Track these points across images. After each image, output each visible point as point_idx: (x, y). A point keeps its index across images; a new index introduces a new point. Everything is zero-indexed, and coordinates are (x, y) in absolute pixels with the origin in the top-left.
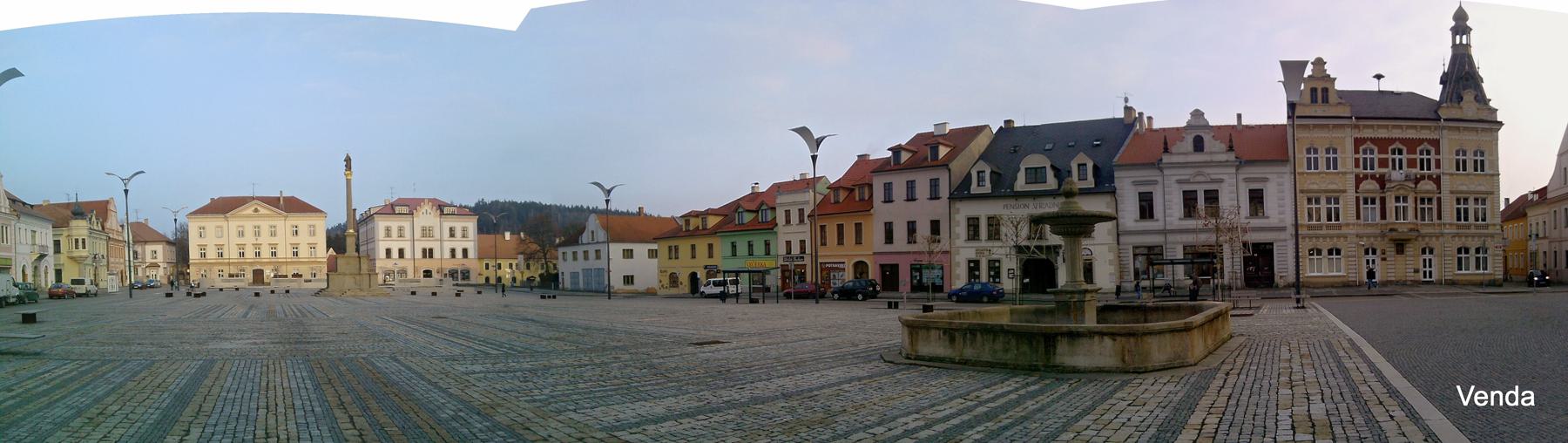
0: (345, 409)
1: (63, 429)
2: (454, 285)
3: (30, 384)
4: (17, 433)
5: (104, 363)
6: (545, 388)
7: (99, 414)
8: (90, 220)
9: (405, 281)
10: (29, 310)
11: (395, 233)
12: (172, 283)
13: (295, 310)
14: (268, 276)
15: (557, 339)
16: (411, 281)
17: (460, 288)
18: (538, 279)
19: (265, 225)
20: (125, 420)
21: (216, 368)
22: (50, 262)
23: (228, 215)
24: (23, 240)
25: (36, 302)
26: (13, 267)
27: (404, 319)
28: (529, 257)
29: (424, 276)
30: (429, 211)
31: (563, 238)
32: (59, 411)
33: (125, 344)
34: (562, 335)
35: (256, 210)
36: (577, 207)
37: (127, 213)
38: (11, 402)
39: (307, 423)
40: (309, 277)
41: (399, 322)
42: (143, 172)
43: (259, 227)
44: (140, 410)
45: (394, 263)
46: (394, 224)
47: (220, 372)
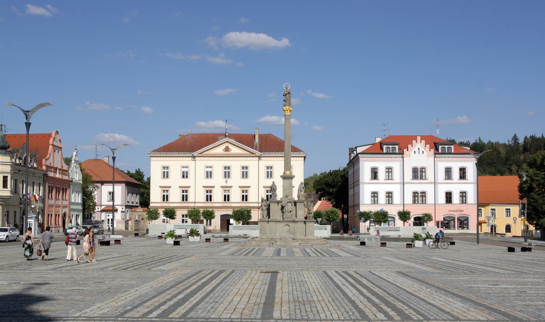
19: (236, 165)
23: (195, 154)
35: (227, 149)
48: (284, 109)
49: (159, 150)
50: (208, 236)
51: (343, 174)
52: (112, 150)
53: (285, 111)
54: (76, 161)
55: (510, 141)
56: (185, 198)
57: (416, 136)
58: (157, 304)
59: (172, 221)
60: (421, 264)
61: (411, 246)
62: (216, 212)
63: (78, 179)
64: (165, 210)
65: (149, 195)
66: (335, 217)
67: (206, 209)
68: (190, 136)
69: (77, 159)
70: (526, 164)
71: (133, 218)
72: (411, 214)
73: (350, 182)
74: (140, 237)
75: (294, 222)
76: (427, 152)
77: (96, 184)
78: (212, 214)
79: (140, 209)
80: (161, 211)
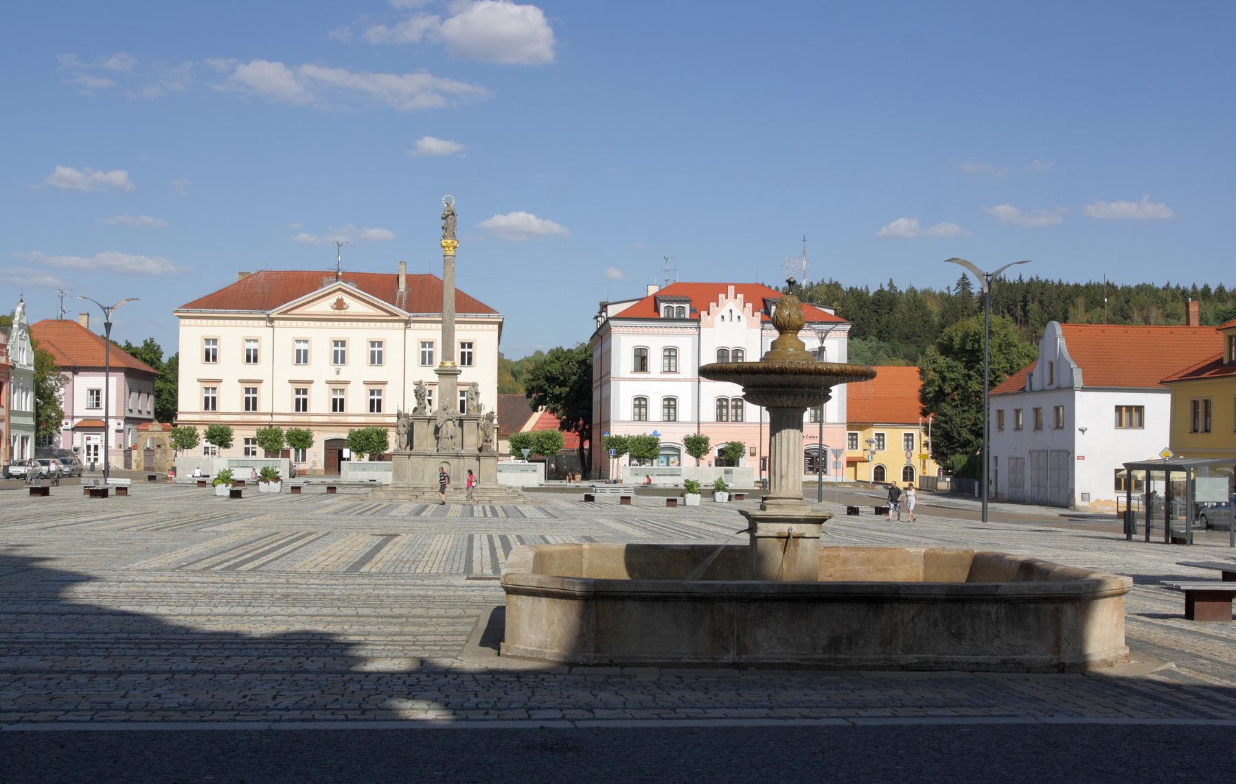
19: (358, 338)
23: (274, 313)
35: (340, 305)
48: (443, 244)
49: (196, 305)
50: (298, 481)
51: (582, 357)
52: (104, 309)
53: (444, 247)
54: (21, 326)
55: (951, 289)
56: (251, 404)
57: (726, 285)
58: (219, 561)
59: (223, 451)
60: (644, 528)
61: (674, 503)
62: (315, 433)
63: (25, 363)
64: (209, 428)
65: (174, 394)
66: (554, 448)
67: (294, 428)
68: (262, 275)
69: (24, 321)
70: (933, 347)
71: (142, 444)
72: (711, 443)
73: (596, 376)
74: (160, 481)
75: (458, 456)
76: (748, 317)
77: (62, 373)
78: (307, 437)
79: (156, 426)
80: (201, 431)
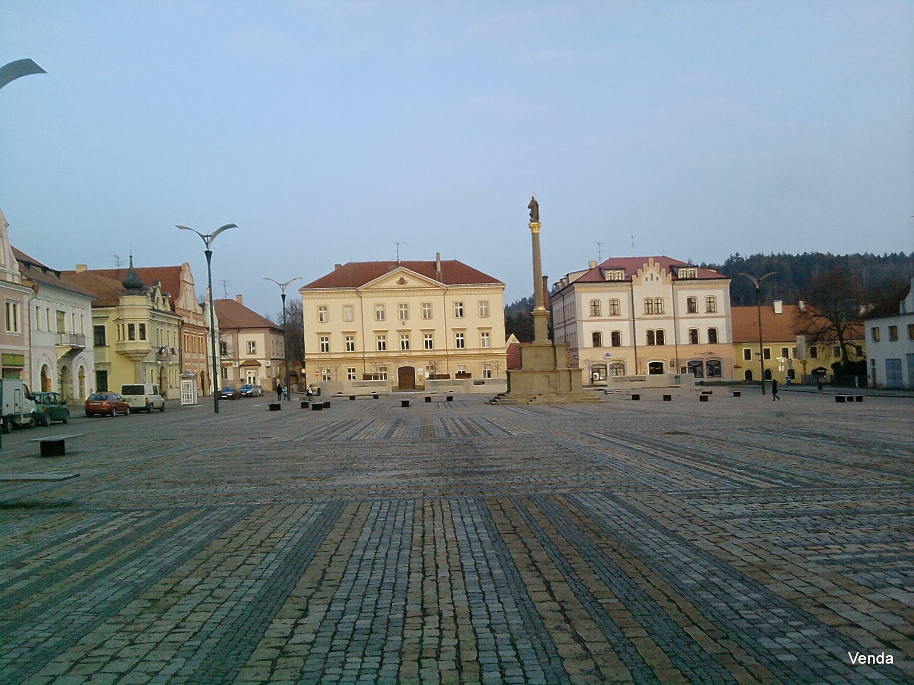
0: (538, 570)
1: (109, 621)
2: (697, 384)
3: (55, 553)
4: (31, 633)
5: (174, 515)
6: (850, 542)
7: (166, 593)
8: (153, 295)
9: (623, 380)
10: (53, 435)
11: (605, 309)
12: (279, 390)
13: (462, 426)
14: (421, 377)
15: (867, 466)
16: (632, 380)
17: (707, 389)
18: (831, 372)
19: (415, 303)
20: (210, 599)
21: (347, 515)
22: (88, 359)
23: (361, 289)
24: (43, 326)
25: (65, 422)
26: (26, 368)
27: (622, 435)
28: (815, 338)
29: (651, 372)
30: (656, 275)
31: (872, 306)
32: (103, 593)
33: (208, 483)
34: (876, 460)
35: (402, 281)
36: (894, 256)
37: (210, 287)
38: (22, 584)
39: (483, 593)
40: (482, 378)
41: (615, 440)
42: (234, 226)
43: (406, 306)
44: (231, 583)
45: (606, 354)
46: (604, 296)
47: (353, 520)
76: (662, 277)
